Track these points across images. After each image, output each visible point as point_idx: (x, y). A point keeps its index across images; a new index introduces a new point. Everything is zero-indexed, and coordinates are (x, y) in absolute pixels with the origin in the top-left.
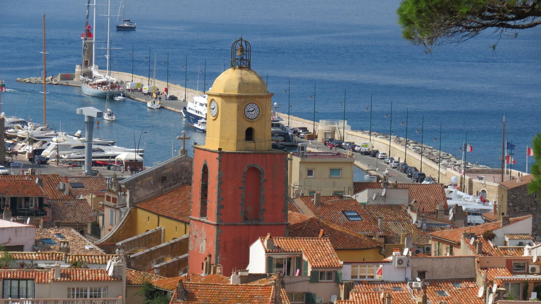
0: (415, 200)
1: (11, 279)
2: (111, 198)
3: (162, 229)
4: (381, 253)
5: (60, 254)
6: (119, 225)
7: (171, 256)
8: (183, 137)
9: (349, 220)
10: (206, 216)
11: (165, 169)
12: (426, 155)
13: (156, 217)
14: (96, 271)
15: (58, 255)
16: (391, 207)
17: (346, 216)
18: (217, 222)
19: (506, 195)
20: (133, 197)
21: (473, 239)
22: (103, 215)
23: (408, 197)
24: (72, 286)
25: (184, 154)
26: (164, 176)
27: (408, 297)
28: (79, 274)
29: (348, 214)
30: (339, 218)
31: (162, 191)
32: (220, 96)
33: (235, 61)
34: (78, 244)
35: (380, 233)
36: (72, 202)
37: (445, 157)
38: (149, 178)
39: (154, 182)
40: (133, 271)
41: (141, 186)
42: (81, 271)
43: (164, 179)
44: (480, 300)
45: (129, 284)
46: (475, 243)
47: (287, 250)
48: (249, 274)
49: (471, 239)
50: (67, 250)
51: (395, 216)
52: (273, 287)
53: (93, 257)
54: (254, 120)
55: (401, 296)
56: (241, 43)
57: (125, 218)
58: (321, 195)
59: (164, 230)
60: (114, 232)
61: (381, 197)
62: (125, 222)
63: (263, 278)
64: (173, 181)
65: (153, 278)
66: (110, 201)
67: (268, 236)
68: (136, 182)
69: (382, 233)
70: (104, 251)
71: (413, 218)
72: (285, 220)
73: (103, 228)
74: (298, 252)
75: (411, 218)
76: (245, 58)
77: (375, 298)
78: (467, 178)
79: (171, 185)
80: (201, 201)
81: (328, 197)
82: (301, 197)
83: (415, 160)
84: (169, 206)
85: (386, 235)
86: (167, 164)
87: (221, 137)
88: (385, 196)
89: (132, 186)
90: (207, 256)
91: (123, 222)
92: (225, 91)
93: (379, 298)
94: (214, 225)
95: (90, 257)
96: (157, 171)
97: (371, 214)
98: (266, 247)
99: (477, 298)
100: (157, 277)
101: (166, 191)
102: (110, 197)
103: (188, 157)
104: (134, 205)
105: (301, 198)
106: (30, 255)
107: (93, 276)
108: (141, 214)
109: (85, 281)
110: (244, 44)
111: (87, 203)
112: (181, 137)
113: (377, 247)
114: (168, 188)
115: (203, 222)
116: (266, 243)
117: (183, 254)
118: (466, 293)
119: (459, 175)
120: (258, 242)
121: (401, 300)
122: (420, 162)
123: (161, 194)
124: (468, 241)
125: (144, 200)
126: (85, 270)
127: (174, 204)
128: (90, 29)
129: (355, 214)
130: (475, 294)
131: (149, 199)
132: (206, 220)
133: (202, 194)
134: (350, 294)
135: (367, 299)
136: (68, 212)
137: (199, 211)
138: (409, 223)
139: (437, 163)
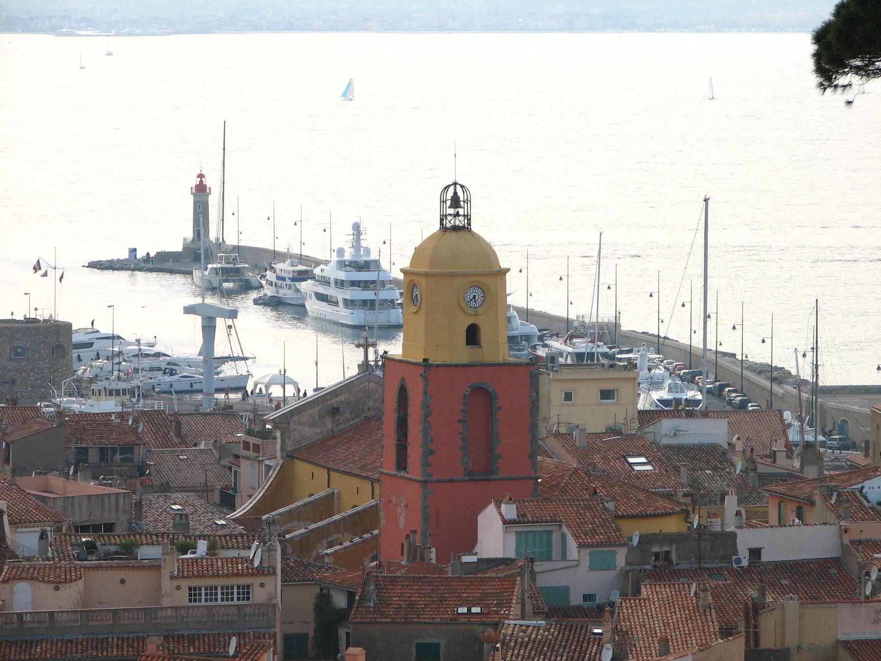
4: (688, 520)
11: (337, 396)
14: (234, 560)
20: (287, 441)
26: (335, 406)
43: (335, 411)
47: (539, 518)
48: (481, 560)
56: (455, 190)
59: (339, 493)
60: (258, 498)
66: (249, 450)
68: (291, 417)
77: (683, 593)
95: (223, 538)
110: (459, 190)
115: (402, 477)
120: (491, 509)
121: (724, 596)
122: (740, 378)
127: (353, 450)
132: (406, 475)
133: (398, 433)
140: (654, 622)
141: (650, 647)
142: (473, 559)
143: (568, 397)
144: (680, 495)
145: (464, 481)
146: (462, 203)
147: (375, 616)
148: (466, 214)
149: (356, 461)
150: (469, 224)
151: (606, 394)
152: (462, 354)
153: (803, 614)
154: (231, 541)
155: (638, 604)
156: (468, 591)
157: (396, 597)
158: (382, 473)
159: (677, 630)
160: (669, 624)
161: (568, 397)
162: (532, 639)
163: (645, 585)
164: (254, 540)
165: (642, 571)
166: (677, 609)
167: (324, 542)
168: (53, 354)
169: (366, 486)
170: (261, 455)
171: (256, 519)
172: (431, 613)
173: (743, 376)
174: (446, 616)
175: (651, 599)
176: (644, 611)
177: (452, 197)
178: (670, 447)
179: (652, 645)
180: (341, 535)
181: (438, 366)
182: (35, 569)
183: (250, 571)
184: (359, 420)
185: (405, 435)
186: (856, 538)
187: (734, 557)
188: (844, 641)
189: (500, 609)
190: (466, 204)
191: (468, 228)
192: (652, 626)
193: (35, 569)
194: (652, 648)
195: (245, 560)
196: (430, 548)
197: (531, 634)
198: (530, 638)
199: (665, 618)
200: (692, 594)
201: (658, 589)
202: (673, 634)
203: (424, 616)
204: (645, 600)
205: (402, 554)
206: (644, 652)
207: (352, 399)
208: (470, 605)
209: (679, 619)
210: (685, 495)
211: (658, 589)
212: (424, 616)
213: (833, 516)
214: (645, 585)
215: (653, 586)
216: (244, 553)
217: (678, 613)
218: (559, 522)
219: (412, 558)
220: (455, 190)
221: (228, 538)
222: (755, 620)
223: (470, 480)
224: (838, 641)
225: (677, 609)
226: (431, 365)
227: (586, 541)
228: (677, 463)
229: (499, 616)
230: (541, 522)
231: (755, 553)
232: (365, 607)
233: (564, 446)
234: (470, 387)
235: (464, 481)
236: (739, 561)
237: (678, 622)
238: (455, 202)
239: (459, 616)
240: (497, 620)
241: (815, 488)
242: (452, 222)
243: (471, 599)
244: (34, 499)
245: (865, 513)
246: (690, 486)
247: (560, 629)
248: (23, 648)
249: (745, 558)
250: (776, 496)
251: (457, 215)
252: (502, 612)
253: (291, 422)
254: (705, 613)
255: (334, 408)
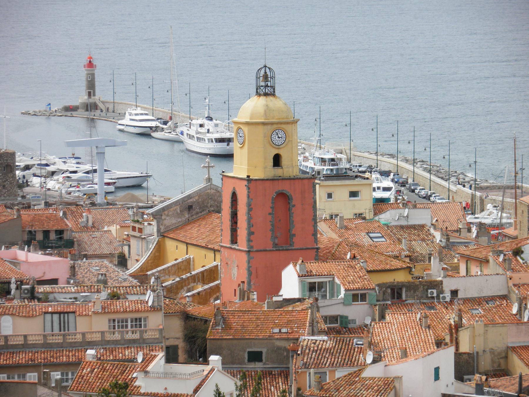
0: (436, 219)
1: (52, 313)
2: (137, 229)
3: (191, 258)
4: (411, 273)
5: (98, 286)
6: (148, 255)
7: (202, 284)
8: (208, 166)
9: (373, 241)
10: (236, 243)
11: (191, 198)
12: (434, 173)
13: (184, 247)
14: (136, 301)
15: (96, 287)
16: (413, 227)
17: (371, 238)
18: (248, 248)
19: (527, 211)
20: (161, 227)
21: (502, 256)
22: (129, 246)
23: (430, 217)
24: (113, 316)
25: (209, 182)
26: (190, 205)
27: (442, 316)
28: (118, 305)
29: (371, 235)
30: (364, 240)
31: (188, 220)
32: (247, 124)
33: (260, 88)
34: (112, 275)
35: (405, 253)
36: (97, 234)
37: (453, 175)
38: (175, 207)
39: (180, 211)
40: (167, 300)
41: (168, 215)
42: (120, 302)
43: (190, 208)
44: (514, 317)
45: (166, 313)
46: (504, 260)
47: (320, 273)
48: (284, 299)
49: (499, 256)
50: (105, 282)
51: (419, 235)
52: (309, 311)
53: (131, 288)
54: (281, 146)
55: (435, 315)
56: (265, 71)
57: (153, 248)
58: (345, 218)
59: (193, 258)
60: (143, 261)
61: (404, 217)
62: (153, 252)
63: (298, 302)
64: (200, 209)
65: (187, 306)
66: (136, 231)
67: (300, 262)
68: (163, 211)
69: (407, 253)
70: (137, 282)
71: (436, 237)
72: (315, 244)
73: (129, 258)
74: (330, 275)
75: (434, 237)
76: (269, 85)
77: (412, 318)
78: (478, 194)
79: (197, 213)
80: (231, 228)
81: (351, 219)
82: (324, 220)
83: (424, 179)
84: (197, 234)
85: (410, 254)
86: (192, 193)
87: (249, 165)
88: (407, 216)
89: (159, 216)
90: (240, 283)
91: (152, 252)
92: (251, 118)
93: (416, 318)
94: (246, 251)
95: (128, 288)
96: (183, 200)
97: (395, 234)
98: (299, 272)
99: (511, 314)
100: (191, 305)
101: (192, 220)
102: (135, 227)
103: (213, 185)
104: (162, 235)
105: (324, 222)
106: (69, 288)
107: (133, 307)
108: (170, 245)
109: (125, 312)
110: (268, 70)
111: (112, 234)
112: (206, 165)
113: (407, 267)
114: (195, 217)
115: (235, 249)
116: (298, 267)
117: (214, 281)
118: (499, 309)
119: (470, 191)
120: (291, 267)
121: (435, 320)
122: (429, 181)
123: (188, 222)
124: (497, 258)
125: (172, 229)
126: (125, 301)
127: (202, 231)
128: (91, 60)
129: (379, 235)
130: (509, 311)
131: (177, 228)
132: (237, 247)
133: (232, 221)
134: (387, 315)
135: (403, 320)
136: (94, 244)
137: (229, 238)
138: (432, 242)
139: (446, 181)
140: (394, 337)
141: (392, 353)
142: (280, 299)
143: (330, 196)
144: (403, 257)
145: (273, 251)
146: (269, 79)
147: (222, 335)
148: (272, 85)
149: (204, 238)
150: (274, 92)
151: (353, 194)
152: (271, 172)
153: (487, 330)
154: (133, 290)
155: (384, 326)
156: (279, 319)
157: (234, 323)
158: (222, 246)
159: (409, 341)
160: (404, 338)
161: (330, 196)
162: (319, 348)
163: (389, 314)
164: (147, 291)
165: (385, 305)
166: (409, 329)
167: (185, 288)
168: (4, 170)
169: (211, 254)
170: (143, 235)
171: (144, 275)
172: (256, 333)
173: (415, 172)
174: (266, 334)
175: (392, 323)
176: (388, 330)
177: (263, 75)
178: (396, 227)
179: (394, 351)
180: (196, 284)
181: (256, 180)
182: (14, 308)
183: (146, 308)
184: (205, 212)
185: (236, 223)
186: (517, 282)
187: (441, 295)
188: (512, 347)
189: (299, 330)
190: (272, 79)
191: (273, 94)
192: (393, 339)
193: (14, 308)
194: (394, 353)
195: (142, 302)
196: (253, 292)
197: (319, 345)
198: (318, 347)
199: (401, 334)
200: (418, 320)
201: (396, 317)
202: (407, 344)
203: (252, 335)
204: (388, 323)
205: (235, 296)
206: (389, 355)
207: (200, 200)
208: (280, 326)
209: (410, 335)
210: (406, 256)
211: (396, 317)
212: (252, 335)
213: (501, 269)
214: (389, 314)
215: (393, 315)
216: (142, 298)
217: (409, 331)
218: (333, 275)
219: (242, 297)
220: (265, 71)
221: (131, 288)
222: (457, 335)
223: (276, 250)
224: (508, 347)
225: (409, 329)
226: (252, 180)
227: (349, 287)
228: (400, 237)
229: (299, 334)
230: (321, 276)
231: (455, 293)
232: (216, 330)
233: (330, 227)
234: (276, 193)
235: (273, 251)
236: (444, 298)
237: (409, 337)
238: (266, 77)
239: (274, 334)
240: (297, 336)
241: (489, 252)
242: (264, 90)
243: (281, 323)
244: (9, 264)
245: (521, 267)
246: (409, 251)
247: (336, 342)
248: (8, 357)
249: (448, 296)
250: (464, 257)
251: (267, 86)
252: (301, 332)
253: (163, 214)
254: (426, 331)
255: (189, 206)
